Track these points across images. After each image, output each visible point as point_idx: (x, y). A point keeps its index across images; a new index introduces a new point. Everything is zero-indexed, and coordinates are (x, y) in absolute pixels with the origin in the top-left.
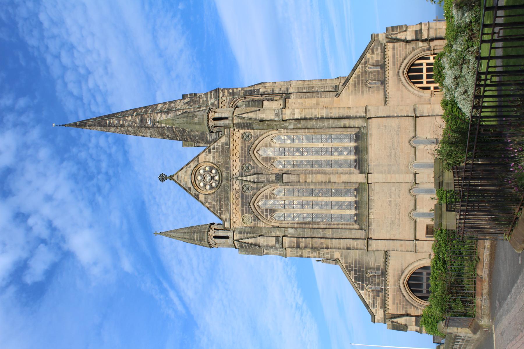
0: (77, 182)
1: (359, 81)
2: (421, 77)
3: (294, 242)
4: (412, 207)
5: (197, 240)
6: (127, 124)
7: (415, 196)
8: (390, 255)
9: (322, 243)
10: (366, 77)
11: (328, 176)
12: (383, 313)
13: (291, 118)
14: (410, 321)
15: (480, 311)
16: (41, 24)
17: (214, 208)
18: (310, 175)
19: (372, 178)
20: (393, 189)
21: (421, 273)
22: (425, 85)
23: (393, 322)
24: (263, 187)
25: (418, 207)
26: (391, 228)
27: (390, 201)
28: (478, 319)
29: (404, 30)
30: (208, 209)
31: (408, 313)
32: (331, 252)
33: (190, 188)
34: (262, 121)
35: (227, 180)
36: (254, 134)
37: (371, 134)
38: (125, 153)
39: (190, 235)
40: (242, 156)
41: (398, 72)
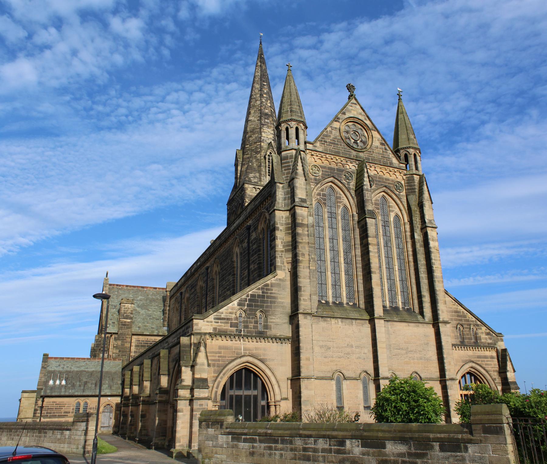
0: (86, 81)
3: (302, 220)
4: (347, 374)
6: (264, 100)
8: (284, 344)
11: (378, 271)
12: (208, 331)
16: (229, 83)
17: (327, 136)
20: (366, 351)
24: (351, 195)
25: (348, 382)
26: (321, 347)
27: (352, 346)
29: (415, 374)
30: (326, 129)
32: (285, 266)
35: (357, 157)
38: (109, 129)
40: (380, 178)
41: (473, 362)
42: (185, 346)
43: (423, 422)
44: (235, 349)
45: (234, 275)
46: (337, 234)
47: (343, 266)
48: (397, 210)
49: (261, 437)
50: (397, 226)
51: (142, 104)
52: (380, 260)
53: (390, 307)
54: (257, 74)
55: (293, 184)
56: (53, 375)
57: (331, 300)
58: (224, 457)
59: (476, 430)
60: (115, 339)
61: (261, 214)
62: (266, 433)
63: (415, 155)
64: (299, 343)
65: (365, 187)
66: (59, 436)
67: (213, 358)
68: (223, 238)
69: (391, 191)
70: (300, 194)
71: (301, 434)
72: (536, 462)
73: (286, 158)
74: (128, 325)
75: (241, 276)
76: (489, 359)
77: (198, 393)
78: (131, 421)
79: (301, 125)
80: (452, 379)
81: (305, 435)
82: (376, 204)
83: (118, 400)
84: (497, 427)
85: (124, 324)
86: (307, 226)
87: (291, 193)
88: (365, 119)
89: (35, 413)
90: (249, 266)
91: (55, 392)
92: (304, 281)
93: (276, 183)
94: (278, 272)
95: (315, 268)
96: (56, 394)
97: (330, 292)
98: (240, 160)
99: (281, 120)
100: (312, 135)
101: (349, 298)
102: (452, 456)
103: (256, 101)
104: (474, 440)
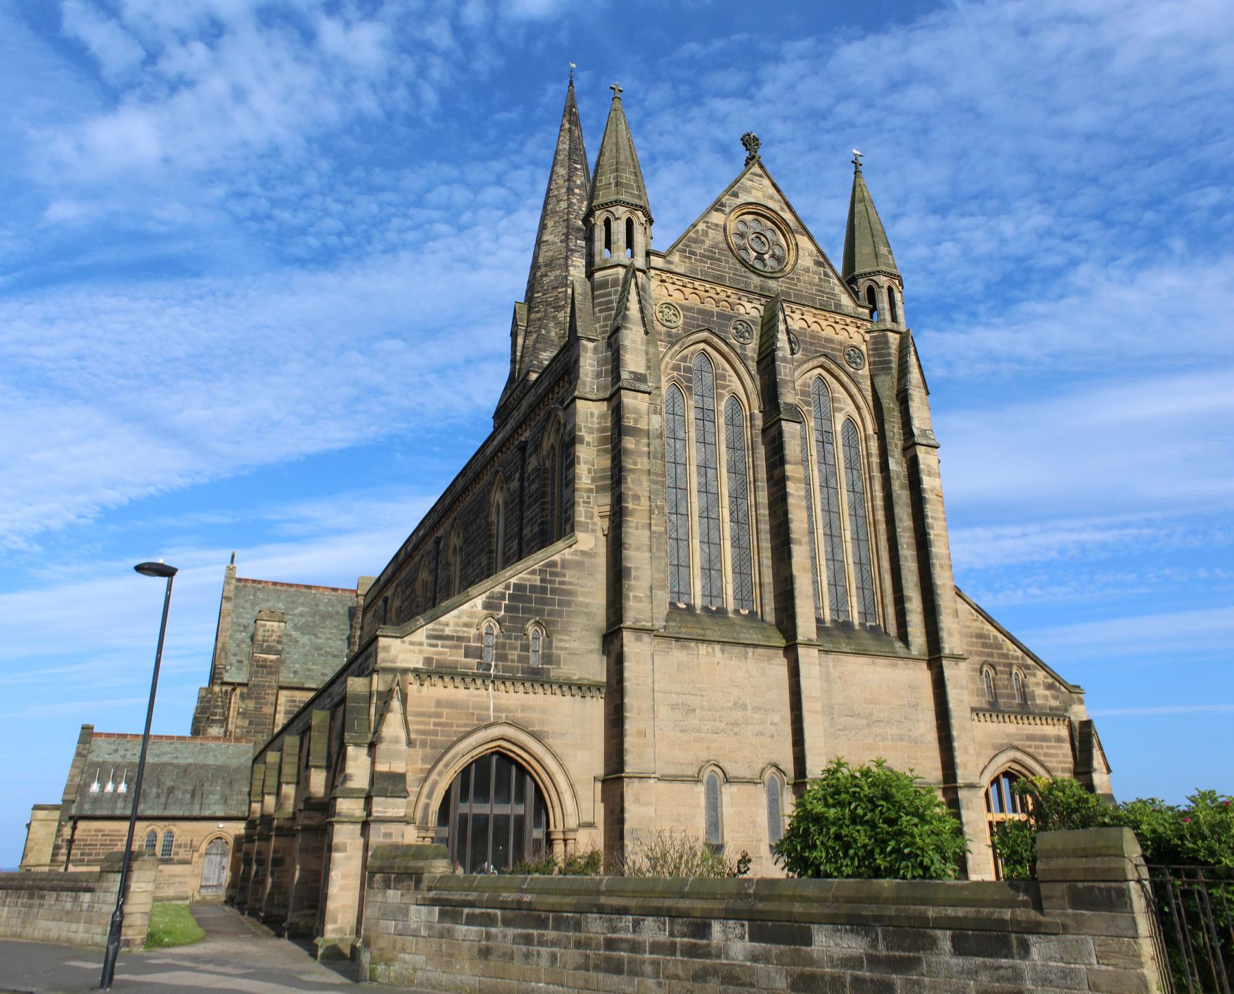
3: (636, 421)
4: (732, 771)
8: (588, 699)
10: (999, 664)
11: (805, 539)
12: (412, 665)
17: (696, 241)
20: (777, 718)
25: (734, 789)
26: (674, 707)
27: (745, 707)
30: (694, 226)
37: (896, 665)
38: (301, 262)
40: (813, 336)
41: (1017, 749)
42: (357, 698)
43: (909, 876)
44: (475, 708)
45: (491, 552)
46: (716, 456)
47: (727, 527)
48: (850, 408)
49: (508, 913)
50: (850, 444)
51: (375, 208)
52: (810, 516)
53: (833, 621)
54: (561, 147)
55: (617, 340)
56: (102, 771)
57: (698, 602)
58: (420, 959)
59: (1051, 898)
60: (243, 697)
61: (549, 413)
62: (519, 902)
63: (890, 290)
64: (622, 698)
65: (780, 354)
66: (69, 906)
67: (422, 727)
68: (470, 474)
69: (838, 365)
70: (633, 362)
71: (603, 905)
72: (1222, 989)
73: (604, 284)
74: (271, 667)
75: (504, 553)
76: (1053, 744)
77: (382, 807)
78: (257, 872)
79: (640, 213)
80: (971, 786)
81: (612, 907)
82: (803, 393)
83: (239, 828)
84: (1109, 890)
85: (263, 665)
86: (647, 433)
87: (613, 360)
88: (782, 209)
89: (55, 855)
90: (521, 530)
91: (101, 808)
92: (637, 557)
93: (579, 339)
94: (580, 535)
95: (662, 529)
96: (105, 812)
97: (698, 585)
98: (522, 324)
99: (595, 203)
100: (662, 238)
101: (741, 599)
102: (985, 966)
103: (559, 201)
104: (1046, 925)
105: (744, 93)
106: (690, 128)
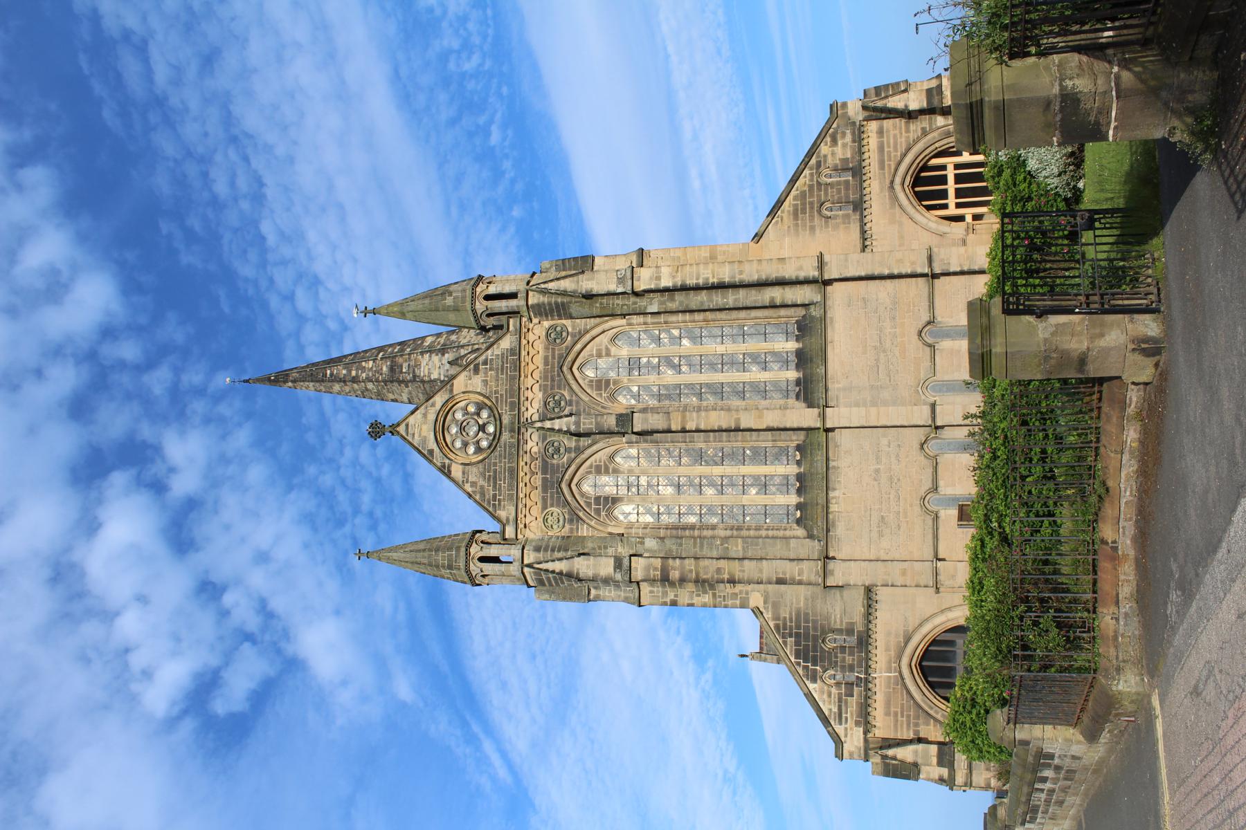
0: (315, 529)
1: (804, 204)
2: (944, 195)
3: (655, 569)
4: (928, 484)
5: (443, 567)
6: (364, 375)
7: (935, 457)
9: (719, 570)
10: (819, 196)
12: (862, 736)
13: (653, 287)
14: (926, 755)
15: (1112, 651)
16: (263, 238)
17: (483, 494)
18: (695, 414)
19: (834, 417)
20: (884, 441)
21: (951, 643)
22: (952, 211)
23: (884, 757)
24: (590, 446)
25: (941, 483)
26: (881, 534)
27: (877, 471)
28: (1106, 677)
30: (470, 496)
31: (922, 735)
32: (741, 592)
33: (431, 452)
34: (589, 296)
35: (512, 431)
36: (574, 328)
37: (832, 319)
39: (430, 556)
40: (546, 378)
41: (892, 182)
51: (342, 416)
105: (142, 50)
106: (194, 104)
